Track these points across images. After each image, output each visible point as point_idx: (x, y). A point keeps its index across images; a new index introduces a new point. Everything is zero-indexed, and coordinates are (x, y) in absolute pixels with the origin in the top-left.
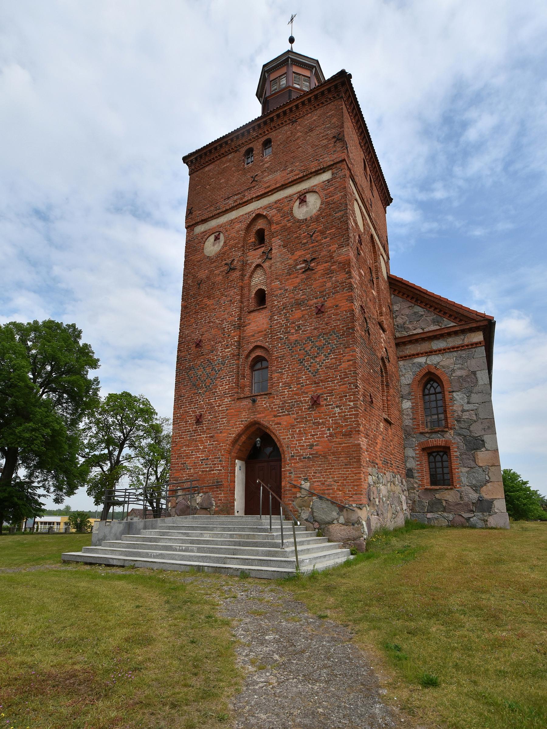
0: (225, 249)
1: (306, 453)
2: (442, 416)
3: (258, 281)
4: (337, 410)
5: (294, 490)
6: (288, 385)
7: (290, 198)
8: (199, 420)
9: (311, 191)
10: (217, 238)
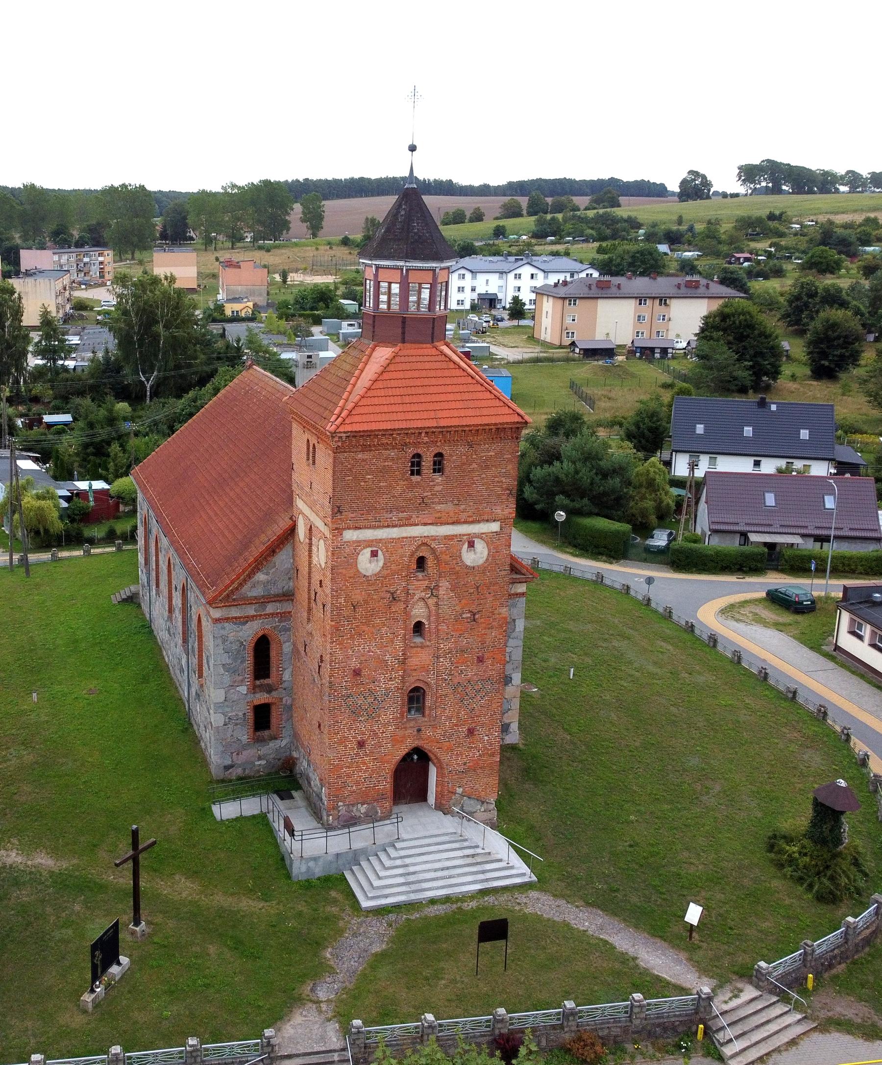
0: (385, 572)
1: (461, 769)
2: (357, 373)
3: (419, 612)
4: (486, 738)
5: (450, 795)
6: (450, 718)
7: (458, 538)
8: (361, 744)
9: (480, 536)
10: (374, 554)
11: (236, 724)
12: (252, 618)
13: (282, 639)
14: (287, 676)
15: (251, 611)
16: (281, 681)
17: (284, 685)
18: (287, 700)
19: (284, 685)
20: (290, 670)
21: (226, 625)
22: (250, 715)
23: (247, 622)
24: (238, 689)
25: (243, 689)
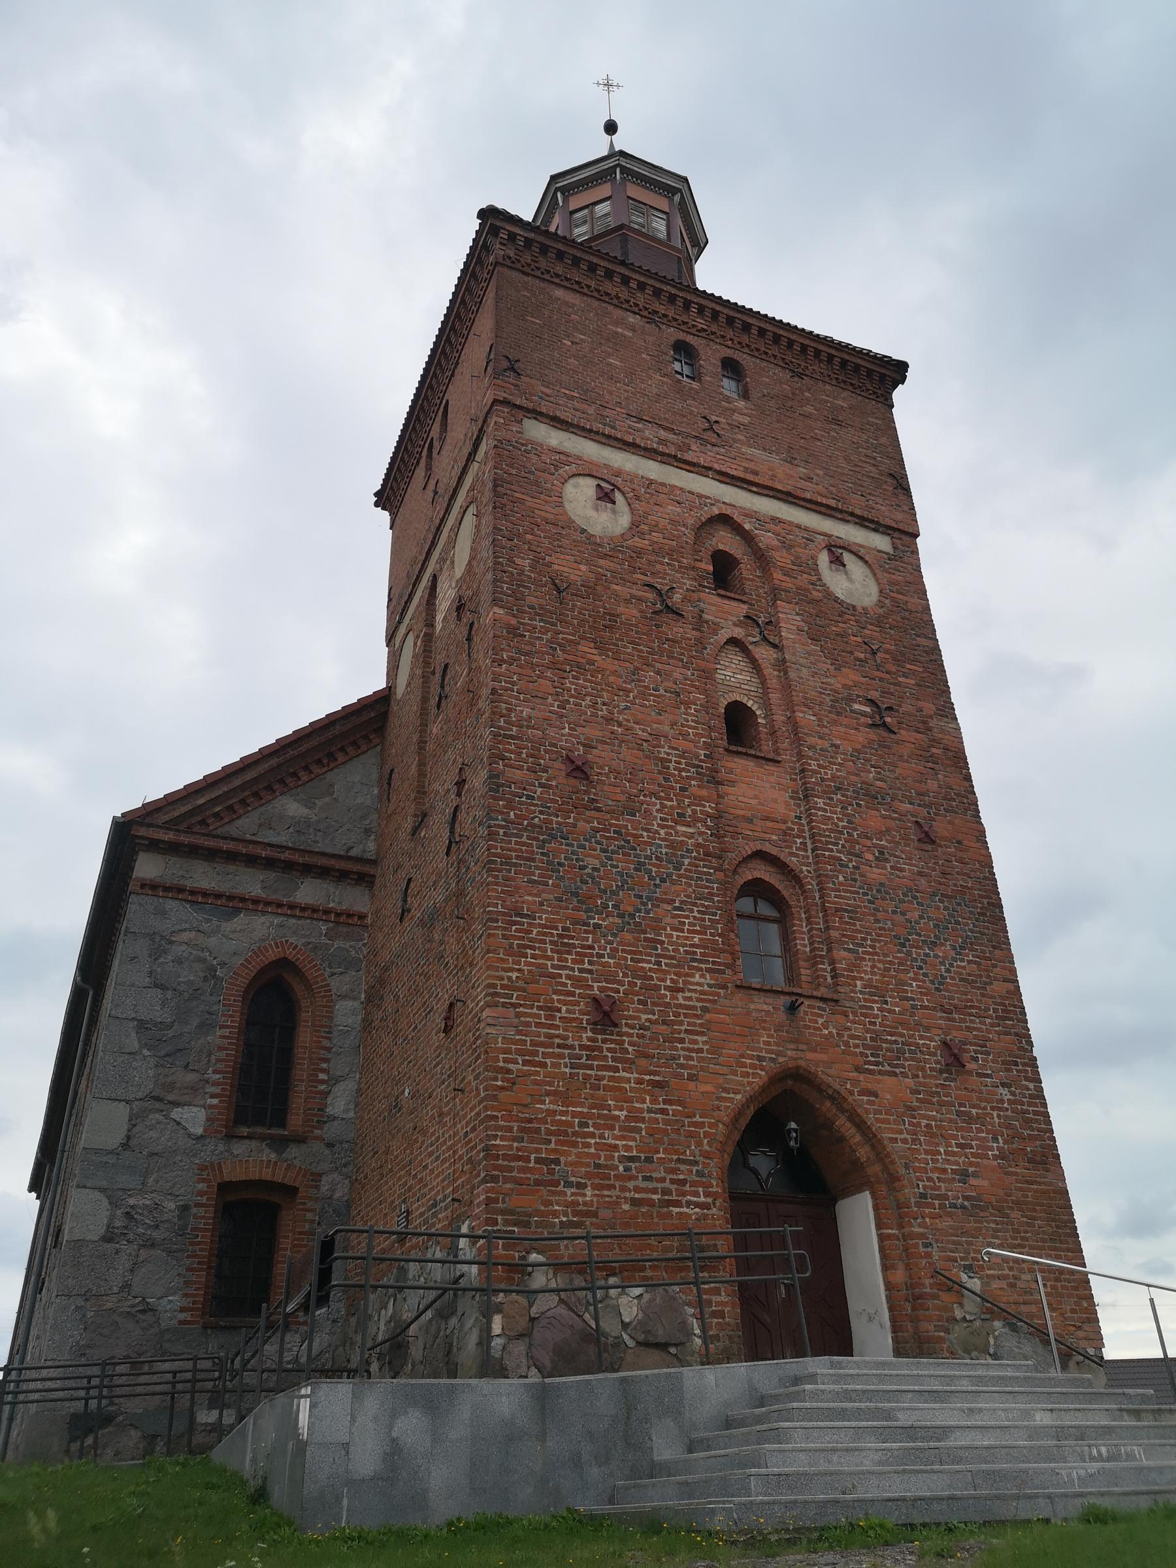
3: (735, 679)
8: (605, 1016)
11: (152, 1245)
12: (256, 904)
13: (334, 983)
14: (340, 1103)
15: (251, 883)
16: (321, 1118)
17: (331, 1131)
18: (334, 1185)
19: (331, 1131)
20: (350, 1085)
21: (171, 904)
22: (204, 1217)
23: (236, 911)
24: (176, 1113)
25: (194, 1118)
